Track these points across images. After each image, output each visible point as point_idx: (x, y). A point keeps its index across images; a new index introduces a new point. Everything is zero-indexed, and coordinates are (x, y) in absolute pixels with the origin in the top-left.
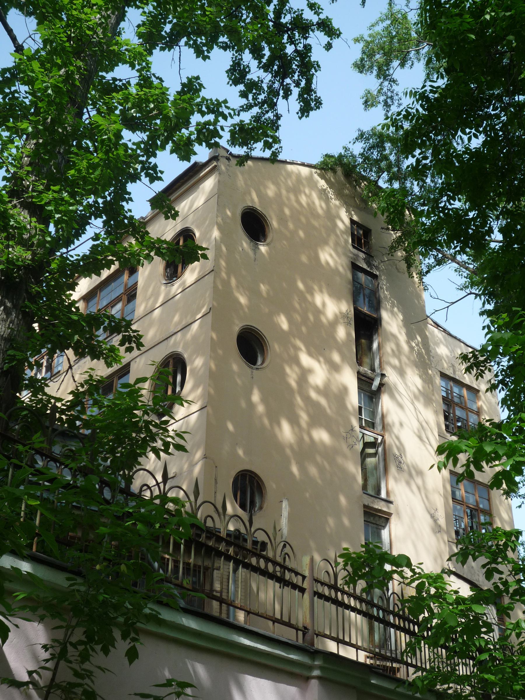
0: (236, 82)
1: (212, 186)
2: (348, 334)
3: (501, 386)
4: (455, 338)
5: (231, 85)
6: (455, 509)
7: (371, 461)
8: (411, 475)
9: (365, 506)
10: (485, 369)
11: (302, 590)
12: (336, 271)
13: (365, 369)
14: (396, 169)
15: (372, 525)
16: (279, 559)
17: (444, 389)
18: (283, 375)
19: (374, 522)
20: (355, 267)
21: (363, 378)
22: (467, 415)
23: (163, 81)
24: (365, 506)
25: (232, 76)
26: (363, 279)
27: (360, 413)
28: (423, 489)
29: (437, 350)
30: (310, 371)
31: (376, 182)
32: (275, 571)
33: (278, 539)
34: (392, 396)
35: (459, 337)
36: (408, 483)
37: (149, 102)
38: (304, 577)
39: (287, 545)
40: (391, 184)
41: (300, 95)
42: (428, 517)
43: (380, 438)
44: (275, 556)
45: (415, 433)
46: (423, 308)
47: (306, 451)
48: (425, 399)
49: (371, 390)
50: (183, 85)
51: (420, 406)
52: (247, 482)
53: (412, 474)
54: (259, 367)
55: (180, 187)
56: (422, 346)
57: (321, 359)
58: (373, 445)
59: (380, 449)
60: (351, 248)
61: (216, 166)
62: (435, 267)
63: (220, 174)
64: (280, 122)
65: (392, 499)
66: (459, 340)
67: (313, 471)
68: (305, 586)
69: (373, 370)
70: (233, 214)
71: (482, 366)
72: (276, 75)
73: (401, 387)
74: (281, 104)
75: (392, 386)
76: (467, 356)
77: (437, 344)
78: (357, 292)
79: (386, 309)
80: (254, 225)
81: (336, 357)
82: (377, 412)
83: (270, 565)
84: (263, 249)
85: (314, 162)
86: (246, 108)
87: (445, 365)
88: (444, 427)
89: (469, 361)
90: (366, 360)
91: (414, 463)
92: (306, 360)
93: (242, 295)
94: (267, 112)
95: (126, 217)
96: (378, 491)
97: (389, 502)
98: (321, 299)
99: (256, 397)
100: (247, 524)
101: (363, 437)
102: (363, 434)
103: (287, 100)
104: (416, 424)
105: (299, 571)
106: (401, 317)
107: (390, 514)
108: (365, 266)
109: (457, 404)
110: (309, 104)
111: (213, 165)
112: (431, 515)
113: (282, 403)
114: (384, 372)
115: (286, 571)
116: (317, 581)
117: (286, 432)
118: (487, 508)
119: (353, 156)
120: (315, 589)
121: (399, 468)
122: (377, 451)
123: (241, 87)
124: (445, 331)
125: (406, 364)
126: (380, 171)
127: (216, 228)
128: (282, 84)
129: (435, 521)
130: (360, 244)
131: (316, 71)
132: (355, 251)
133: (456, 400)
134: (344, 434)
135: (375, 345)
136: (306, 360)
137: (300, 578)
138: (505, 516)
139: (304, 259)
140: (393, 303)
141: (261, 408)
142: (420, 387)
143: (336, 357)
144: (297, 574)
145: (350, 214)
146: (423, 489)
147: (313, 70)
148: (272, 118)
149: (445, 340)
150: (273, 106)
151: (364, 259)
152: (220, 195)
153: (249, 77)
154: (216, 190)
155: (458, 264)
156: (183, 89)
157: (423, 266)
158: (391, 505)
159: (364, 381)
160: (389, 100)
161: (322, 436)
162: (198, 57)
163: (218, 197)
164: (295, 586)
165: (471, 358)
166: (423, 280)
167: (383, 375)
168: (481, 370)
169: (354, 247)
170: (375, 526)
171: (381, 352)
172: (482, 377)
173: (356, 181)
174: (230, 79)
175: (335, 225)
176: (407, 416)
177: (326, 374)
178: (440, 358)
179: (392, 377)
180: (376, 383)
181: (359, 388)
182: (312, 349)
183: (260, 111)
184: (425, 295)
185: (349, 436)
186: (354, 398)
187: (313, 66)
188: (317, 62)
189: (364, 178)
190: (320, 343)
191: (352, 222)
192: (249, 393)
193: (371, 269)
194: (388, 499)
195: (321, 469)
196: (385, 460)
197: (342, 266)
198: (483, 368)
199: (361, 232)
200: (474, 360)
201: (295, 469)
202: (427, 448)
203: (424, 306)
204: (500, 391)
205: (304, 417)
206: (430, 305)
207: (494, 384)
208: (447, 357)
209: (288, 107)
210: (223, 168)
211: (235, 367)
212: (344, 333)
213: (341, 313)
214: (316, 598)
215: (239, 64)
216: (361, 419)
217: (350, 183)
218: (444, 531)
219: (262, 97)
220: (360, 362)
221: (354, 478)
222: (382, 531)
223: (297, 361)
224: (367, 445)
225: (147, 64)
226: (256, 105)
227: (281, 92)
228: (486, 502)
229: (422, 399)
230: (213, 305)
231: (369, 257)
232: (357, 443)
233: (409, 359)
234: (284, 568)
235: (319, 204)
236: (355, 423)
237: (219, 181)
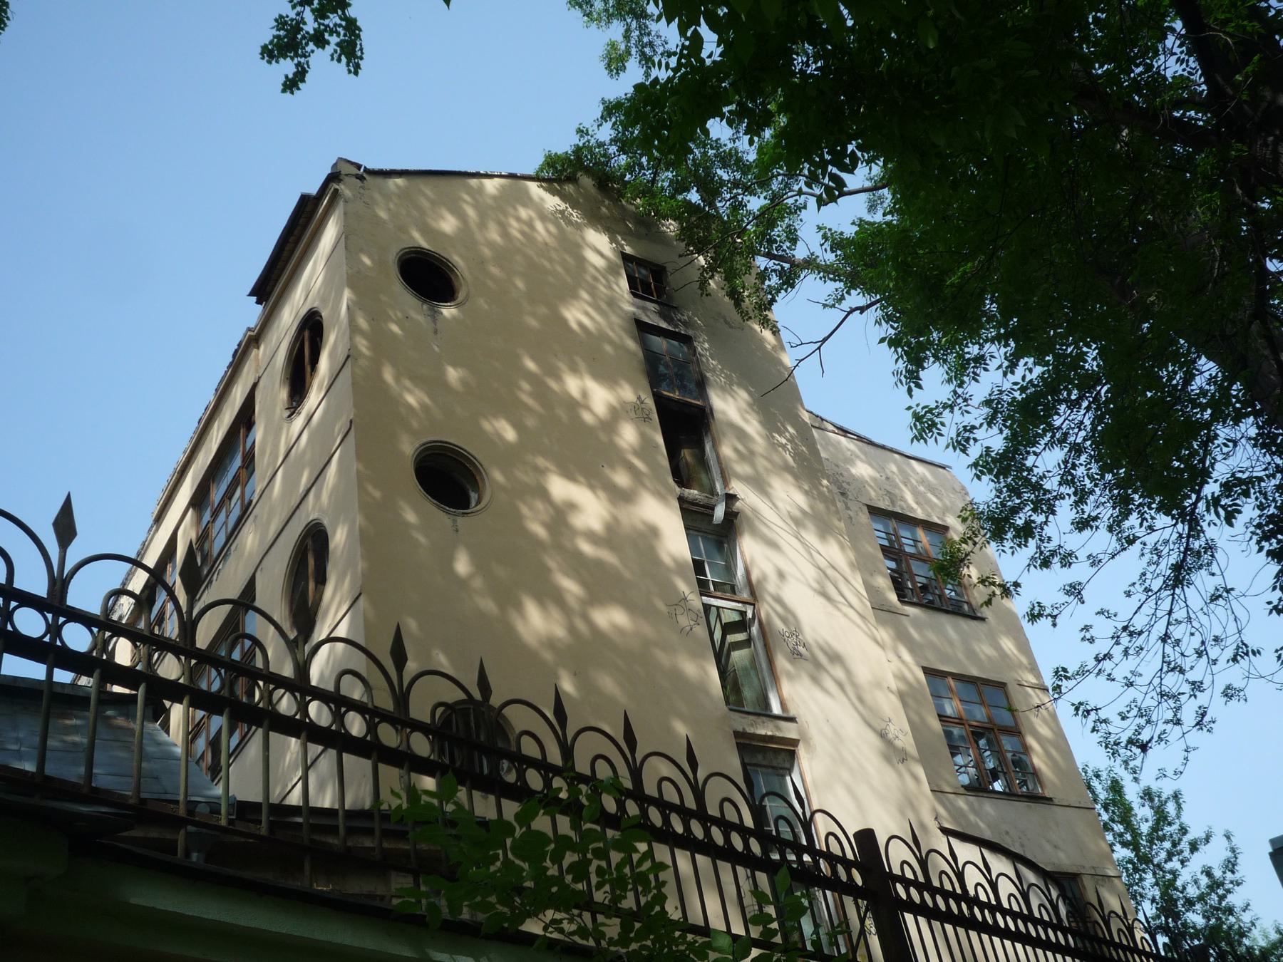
4: (883, 447)
7: (738, 656)
8: (818, 665)
9: (737, 734)
12: (602, 337)
15: (764, 770)
17: (883, 535)
18: (517, 520)
19: (764, 763)
20: (642, 329)
24: (737, 734)
29: (853, 471)
30: (572, 506)
34: (755, 533)
35: (889, 444)
36: (815, 680)
45: (811, 587)
47: (587, 649)
48: (818, 527)
49: (715, 529)
51: (811, 537)
53: (820, 662)
55: (292, 252)
59: (755, 629)
65: (792, 713)
66: (891, 450)
67: (608, 684)
75: (749, 513)
77: (850, 461)
78: (655, 371)
84: (448, 312)
87: (873, 494)
91: (821, 642)
104: (811, 573)
107: (795, 743)
109: (912, 556)
113: (523, 571)
121: (795, 656)
124: (860, 438)
125: (767, 470)
136: (560, 488)
138: (1044, 731)
142: (806, 508)
143: (622, 479)
149: (865, 453)
160: (647, 50)
161: (612, 618)
167: (731, 498)
175: (582, 260)
176: (793, 563)
178: (860, 483)
179: (747, 496)
180: (719, 512)
181: (687, 528)
186: (675, 541)
190: (587, 454)
192: (449, 560)
193: (676, 326)
196: (766, 646)
202: (845, 615)
205: (570, 586)
208: (875, 480)
211: (411, 517)
217: (610, 198)
218: (913, 758)
221: (702, 688)
223: (544, 494)
228: (1007, 715)
229: (810, 525)
231: (667, 309)
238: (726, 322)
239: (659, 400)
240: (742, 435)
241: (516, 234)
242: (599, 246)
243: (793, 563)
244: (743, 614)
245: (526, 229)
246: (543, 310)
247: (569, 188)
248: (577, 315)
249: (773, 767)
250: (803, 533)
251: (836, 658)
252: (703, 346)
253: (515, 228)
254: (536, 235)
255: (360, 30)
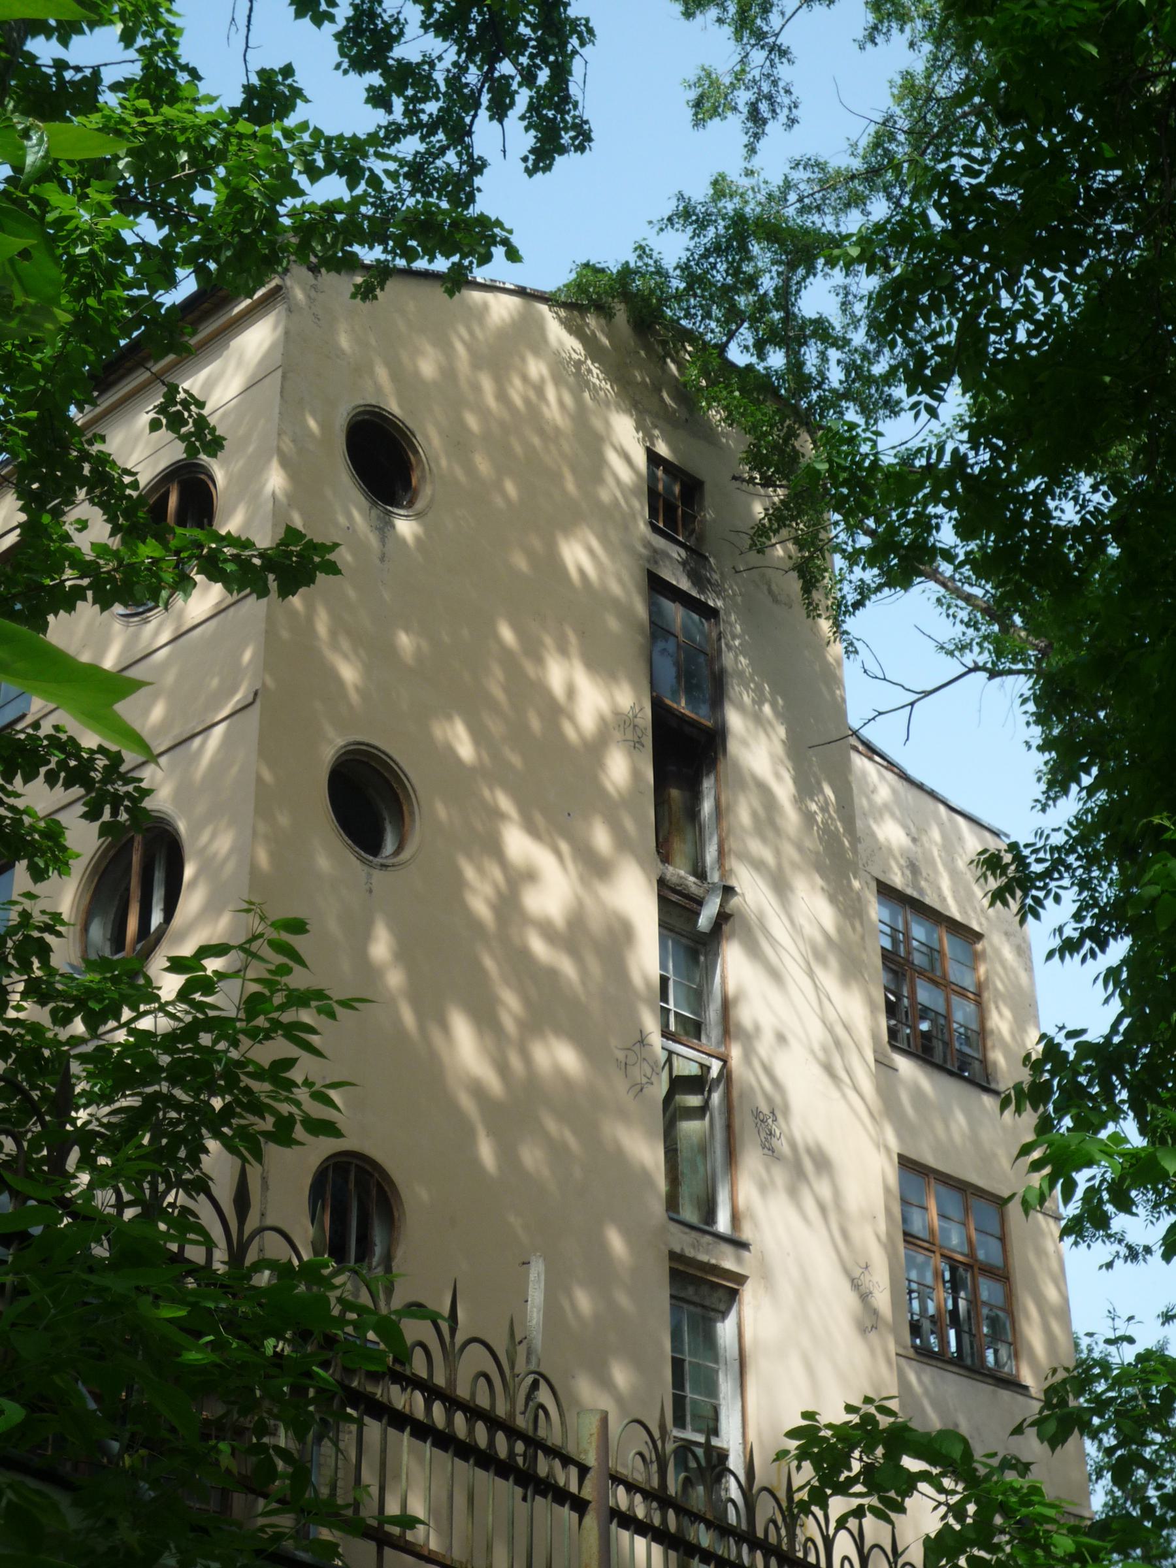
0: (360, 64)
1: (266, 345)
2: (636, 774)
3: (1088, 944)
4: (920, 787)
5: (346, 72)
6: (910, 1263)
7: (691, 1128)
9: (674, 1256)
10: (1046, 896)
11: (580, 1506)
13: (679, 872)
14: (776, 315)
15: (692, 1308)
16: (521, 1422)
17: (887, 930)
19: (696, 1299)
20: (656, 586)
21: (674, 897)
22: (948, 1001)
23: (200, 78)
24: (674, 1256)
25: (350, 49)
26: (679, 621)
27: (664, 997)
28: (832, 1211)
30: (530, 876)
31: (723, 348)
32: (511, 1453)
33: (521, 1366)
34: (753, 950)
35: (930, 783)
36: (793, 1193)
37: (177, 147)
38: (583, 1470)
39: (542, 1382)
40: (762, 356)
41: (533, 107)
42: (845, 1285)
43: (716, 1066)
44: (512, 1414)
45: (812, 1052)
46: (839, 710)
49: (695, 930)
50: (249, 89)
51: (829, 981)
52: (352, 1186)
53: (807, 1167)
54: (390, 861)
56: (836, 812)
57: (564, 847)
58: (697, 1083)
59: (716, 1097)
60: (643, 527)
61: (278, 288)
62: (879, 589)
63: (290, 310)
64: (478, 181)
65: (747, 1234)
66: (932, 794)
67: (531, 1157)
68: (588, 1493)
69: (700, 874)
70: (325, 428)
71: (1039, 889)
72: (470, 48)
73: (778, 927)
74: (485, 134)
76: (999, 858)
77: (878, 813)
79: (741, 708)
80: (382, 457)
81: (602, 839)
82: (710, 992)
83: (501, 1438)
84: (405, 527)
85: (548, 285)
86: (386, 138)
88: (885, 1037)
89: (1004, 873)
90: (681, 848)
92: (518, 843)
93: (346, 657)
94: (443, 151)
95: (85, 456)
96: (709, 1213)
97: (741, 1245)
98: (561, 673)
99: (381, 948)
100: (445, 1326)
101: (669, 1060)
102: (671, 1053)
103: (501, 121)
104: (817, 1032)
105: (571, 1450)
106: (782, 731)
107: (741, 1279)
108: (684, 584)
109: (921, 973)
110: (557, 133)
111: (273, 284)
112: (853, 1280)
114: (733, 882)
115: (540, 1454)
116: (617, 1479)
117: (466, 1048)
118: (996, 1260)
119: (660, 272)
120: (611, 1503)
122: (707, 1102)
123: (375, 78)
124: (891, 766)
126: (733, 317)
127: (275, 464)
128: (488, 77)
129: (864, 1297)
130: (671, 521)
131: (583, 44)
132: (660, 542)
133: (918, 959)
134: (620, 1055)
135: (707, 807)
136: (518, 843)
137: (574, 1471)
139: (521, 562)
140: (759, 690)
141: (395, 979)
143: (602, 839)
144: (567, 1460)
145: (648, 436)
146: (832, 1211)
147: (574, 41)
148: (456, 167)
150: (460, 134)
151: (684, 564)
152: (288, 371)
153: (399, 52)
154: (278, 359)
155: (944, 585)
156: (247, 102)
157: (846, 588)
158: (746, 1254)
159: (676, 907)
161: (560, 1057)
162: (299, 14)
163: (284, 377)
164: (561, 1496)
165: (1008, 865)
166: (845, 627)
167: (728, 891)
168: (1035, 898)
169: (655, 529)
170: (699, 1310)
171: (725, 824)
172: (1037, 916)
173: (664, 343)
174: (342, 54)
175: (600, 462)
176: (800, 1018)
177: (571, 887)
178: (879, 850)
179: (752, 892)
181: (663, 925)
182: (539, 819)
183: (422, 148)
184: (850, 672)
185: (631, 1061)
186: (647, 956)
187: (574, 31)
188: (587, 20)
189: (689, 336)
190: (558, 794)
191: (653, 458)
192: (364, 937)
193: (702, 591)
194: (736, 1236)
195: (556, 1150)
196: (729, 1127)
197: (620, 581)
198: (1041, 894)
199: (677, 489)
200: (1017, 870)
201: (486, 1152)
202: (844, 1096)
203: (844, 700)
204: (1084, 960)
205: (511, 1002)
206: (860, 699)
207: (1069, 939)
209: (500, 140)
210: (299, 295)
211: (323, 863)
212: (623, 770)
213: (617, 713)
214: (614, 1526)
215: (373, 15)
216: (665, 1012)
217: (648, 348)
219: (432, 107)
220: (664, 852)
222: (719, 1325)
223: (495, 849)
224: (679, 1084)
225: (168, 34)
226: (411, 129)
227: (485, 99)
228: (994, 1245)
229: (833, 961)
230: (264, 684)
232: (654, 1079)
233: (800, 848)
234: (535, 1444)
235: (555, 406)
236: (651, 1025)
237: (287, 333)
238: (770, 591)
239: (659, 709)
240: (764, 790)
241: (518, 401)
242: (627, 443)
243: (800, 1018)
244: (706, 1068)
245: (532, 395)
246: (537, 543)
247: (592, 322)
248: (579, 555)
249: (703, 1307)
250: (819, 972)
251: (823, 1163)
252: (735, 626)
253: (516, 392)
254: (545, 410)
255: (498, 223)
